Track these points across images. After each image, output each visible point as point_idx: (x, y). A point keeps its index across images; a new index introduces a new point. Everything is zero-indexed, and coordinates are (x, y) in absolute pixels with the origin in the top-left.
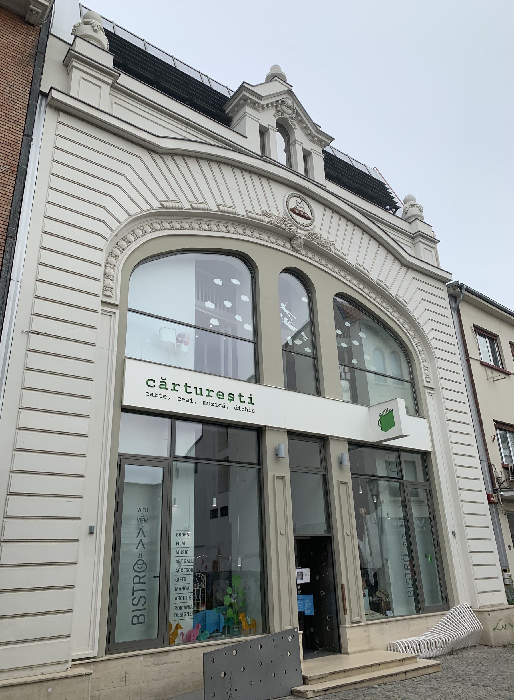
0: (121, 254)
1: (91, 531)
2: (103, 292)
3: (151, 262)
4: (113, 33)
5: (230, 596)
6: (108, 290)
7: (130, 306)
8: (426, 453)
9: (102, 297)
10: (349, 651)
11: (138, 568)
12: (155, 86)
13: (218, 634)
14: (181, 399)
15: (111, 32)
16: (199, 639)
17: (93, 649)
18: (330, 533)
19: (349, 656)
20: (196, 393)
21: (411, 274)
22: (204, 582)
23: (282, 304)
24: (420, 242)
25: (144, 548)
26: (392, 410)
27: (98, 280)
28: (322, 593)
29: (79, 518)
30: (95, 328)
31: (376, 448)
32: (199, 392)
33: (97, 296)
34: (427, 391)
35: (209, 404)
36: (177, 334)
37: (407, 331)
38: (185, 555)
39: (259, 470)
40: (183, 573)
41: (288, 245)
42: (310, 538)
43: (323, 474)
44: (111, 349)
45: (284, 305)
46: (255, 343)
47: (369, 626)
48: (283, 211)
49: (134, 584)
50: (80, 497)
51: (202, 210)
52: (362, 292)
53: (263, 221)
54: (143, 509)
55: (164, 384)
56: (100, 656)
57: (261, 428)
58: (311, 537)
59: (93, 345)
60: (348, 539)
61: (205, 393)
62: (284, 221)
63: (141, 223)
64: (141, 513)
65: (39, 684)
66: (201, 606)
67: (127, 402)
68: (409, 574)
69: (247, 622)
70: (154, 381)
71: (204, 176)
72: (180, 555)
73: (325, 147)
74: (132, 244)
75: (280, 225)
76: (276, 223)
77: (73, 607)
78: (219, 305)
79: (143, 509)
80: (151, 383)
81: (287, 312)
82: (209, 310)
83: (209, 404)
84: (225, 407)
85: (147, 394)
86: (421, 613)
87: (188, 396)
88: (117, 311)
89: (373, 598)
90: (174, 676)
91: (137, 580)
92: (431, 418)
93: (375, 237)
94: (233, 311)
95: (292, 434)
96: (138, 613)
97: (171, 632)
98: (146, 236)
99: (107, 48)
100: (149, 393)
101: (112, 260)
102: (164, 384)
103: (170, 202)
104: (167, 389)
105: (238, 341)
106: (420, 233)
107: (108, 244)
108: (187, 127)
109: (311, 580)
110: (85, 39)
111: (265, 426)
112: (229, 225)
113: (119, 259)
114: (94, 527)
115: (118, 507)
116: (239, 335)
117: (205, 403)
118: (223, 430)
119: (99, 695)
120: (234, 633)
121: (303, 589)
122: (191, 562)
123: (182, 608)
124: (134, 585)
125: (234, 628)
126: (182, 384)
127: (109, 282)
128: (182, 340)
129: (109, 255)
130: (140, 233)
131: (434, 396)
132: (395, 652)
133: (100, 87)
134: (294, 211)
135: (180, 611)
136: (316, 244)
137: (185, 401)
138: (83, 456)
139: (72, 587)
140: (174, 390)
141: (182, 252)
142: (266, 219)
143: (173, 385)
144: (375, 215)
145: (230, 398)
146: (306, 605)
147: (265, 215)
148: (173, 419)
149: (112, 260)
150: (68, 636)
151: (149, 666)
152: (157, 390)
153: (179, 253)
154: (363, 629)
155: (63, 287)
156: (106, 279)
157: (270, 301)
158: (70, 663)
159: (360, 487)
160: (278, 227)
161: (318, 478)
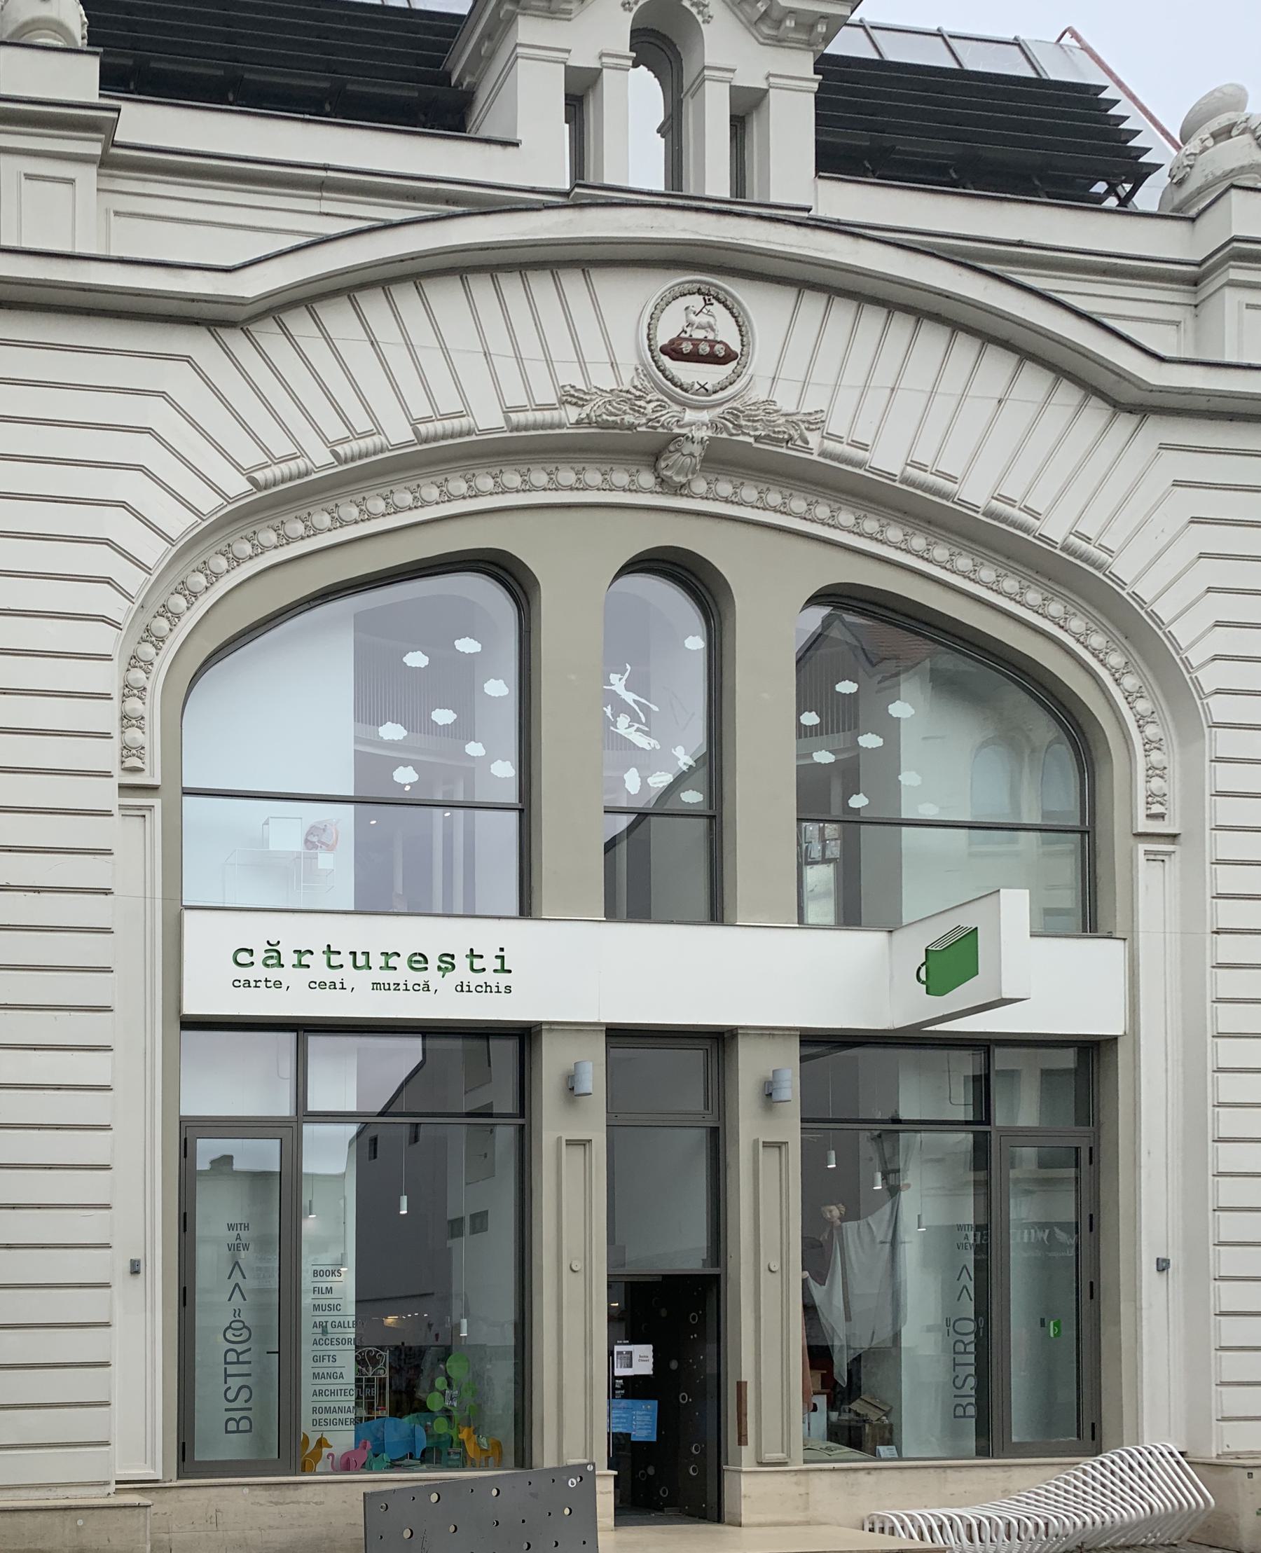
0: (157, 654)
1: (135, 1269)
2: (123, 762)
3: (239, 652)
4: (873, 61)
5: (443, 1393)
6: (134, 755)
7: (187, 784)
8: (1099, 1041)
9: (119, 776)
10: (744, 1521)
11: (234, 1335)
12: (231, 98)
13: (412, 1462)
14: (317, 985)
15: (946, 69)
16: (366, 1467)
17: (154, 1467)
18: (718, 1265)
19: (743, 1530)
20: (355, 966)
21: (1158, 430)
22: (385, 1365)
23: (614, 678)
24: (1233, 284)
25: (245, 1300)
26: (976, 928)
27: (106, 736)
28: (684, 1398)
29: (107, 1246)
30: (108, 852)
31: (946, 1045)
32: (361, 961)
33: (107, 775)
34: (1142, 847)
35: (387, 987)
36: (306, 829)
37: (1096, 656)
38: (332, 1313)
39: (522, 1127)
40: (330, 1347)
41: (647, 479)
42: (661, 1277)
43: (711, 1127)
44: (148, 895)
45: (620, 679)
46: (521, 811)
47: (812, 1475)
48: (636, 362)
49: (955, 1353)
50: (107, 1207)
51: (367, 455)
52: (920, 561)
53: (560, 426)
54: (239, 1226)
55: (274, 956)
56: (167, 1479)
57: (531, 1028)
58: (663, 1275)
59: (107, 892)
60: (770, 1285)
61: (377, 961)
62: (632, 399)
63: (199, 555)
64: (235, 1233)
65: (62, 1513)
66: (377, 1410)
67: (193, 1006)
68: (971, 1364)
69: (478, 1444)
70: (251, 952)
71: (372, 343)
72: (321, 1313)
73: (827, 39)
74: (183, 619)
75: (618, 419)
76: (605, 417)
77: (110, 1398)
78: (418, 723)
79: (239, 1226)
80: (244, 958)
81: (629, 697)
82: (392, 745)
83: (387, 987)
84: (428, 990)
85: (237, 984)
86: (993, 1457)
87: (335, 976)
88: (156, 802)
89: (840, 1415)
90: (311, 1526)
91: (232, 1357)
92: (1141, 935)
93: (1006, 337)
94: (463, 730)
95: (618, 1034)
96: (237, 1415)
97: (308, 1452)
98: (217, 585)
99: (83, 38)
100: (240, 981)
101: (138, 675)
102: (275, 954)
103: (275, 464)
104: (283, 966)
105: (478, 812)
106: (1235, 244)
107: (122, 638)
108: (320, 199)
109: (654, 1369)
110: (22, 41)
111: (541, 1023)
112: (449, 477)
113: (154, 670)
114: (139, 1261)
115: (186, 1222)
116: (479, 798)
117: (376, 986)
118: (478, 1044)
119: (170, 1540)
120: (450, 1463)
121: (631, 1388)
122: (346, 1325)
123: (328, 1410)
124: (227, 1366)
125: (449, 1454)
126: (319, 949)
127: (134, 735)
128: (319, 841)
129: (130, 664)
130: (200, 584)
131: (1173, 865)
132: (886, 1535)
133: (71, 181)
134: (673, 350)
135: (324, 1416)
136: (751, 440)
137: (327, 987)
138: (106, 1128)
139: (106, 1364)
140: (300, 965)
141: (313, 604)
142: (573, 414)
143: (383, 958)
144: (1020, 244)
145: (443, 966)
146: (635, 1420)
147: (570, 399)
148: (301, 1033)
149: (138, 675)
150: (107, 1444)
151: (261, 1505)
152: (258, 972)
153: (307, 606)
154: (794, 1478)
155: (88, 775)
156: (127, 728)
157: (573, 677)
158: (113, 1487)
159: (833, 1153)
160: (614, 425)
161: (696, 1139)
